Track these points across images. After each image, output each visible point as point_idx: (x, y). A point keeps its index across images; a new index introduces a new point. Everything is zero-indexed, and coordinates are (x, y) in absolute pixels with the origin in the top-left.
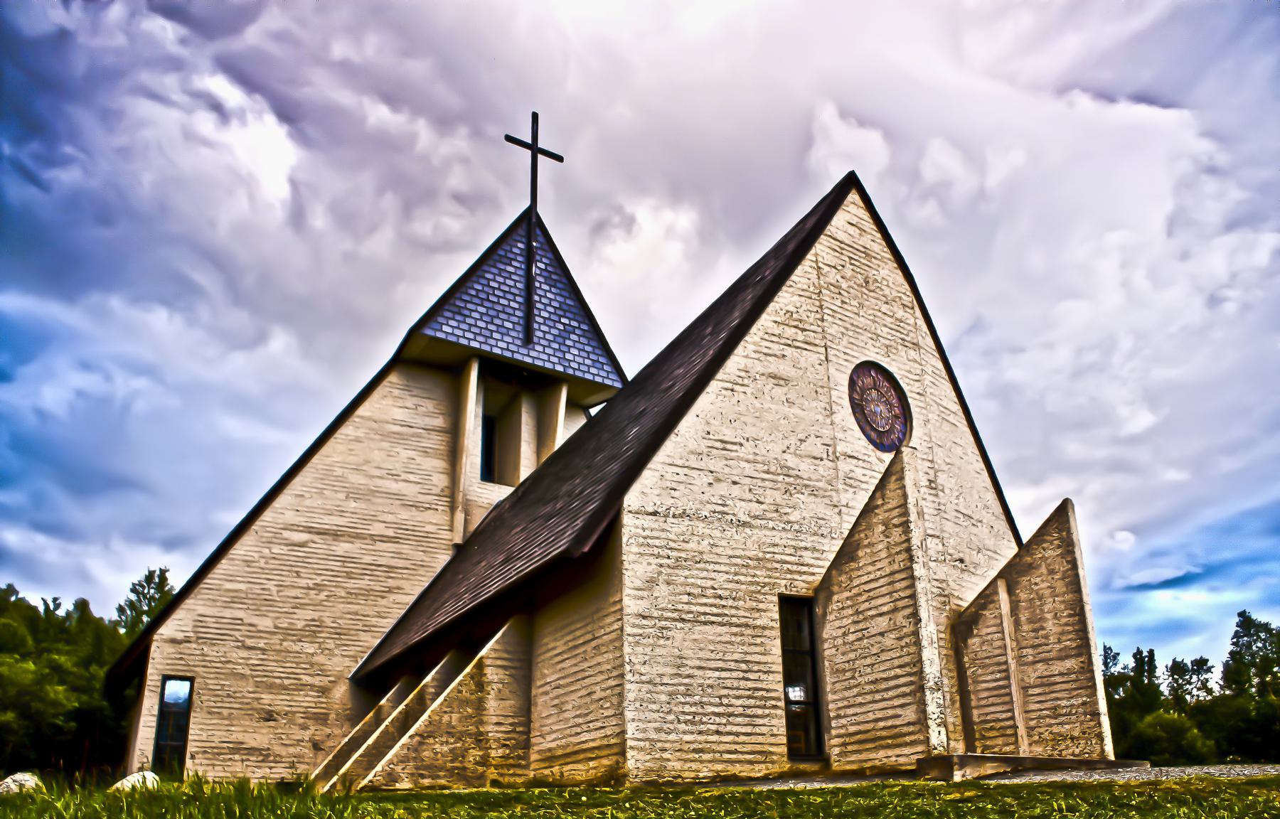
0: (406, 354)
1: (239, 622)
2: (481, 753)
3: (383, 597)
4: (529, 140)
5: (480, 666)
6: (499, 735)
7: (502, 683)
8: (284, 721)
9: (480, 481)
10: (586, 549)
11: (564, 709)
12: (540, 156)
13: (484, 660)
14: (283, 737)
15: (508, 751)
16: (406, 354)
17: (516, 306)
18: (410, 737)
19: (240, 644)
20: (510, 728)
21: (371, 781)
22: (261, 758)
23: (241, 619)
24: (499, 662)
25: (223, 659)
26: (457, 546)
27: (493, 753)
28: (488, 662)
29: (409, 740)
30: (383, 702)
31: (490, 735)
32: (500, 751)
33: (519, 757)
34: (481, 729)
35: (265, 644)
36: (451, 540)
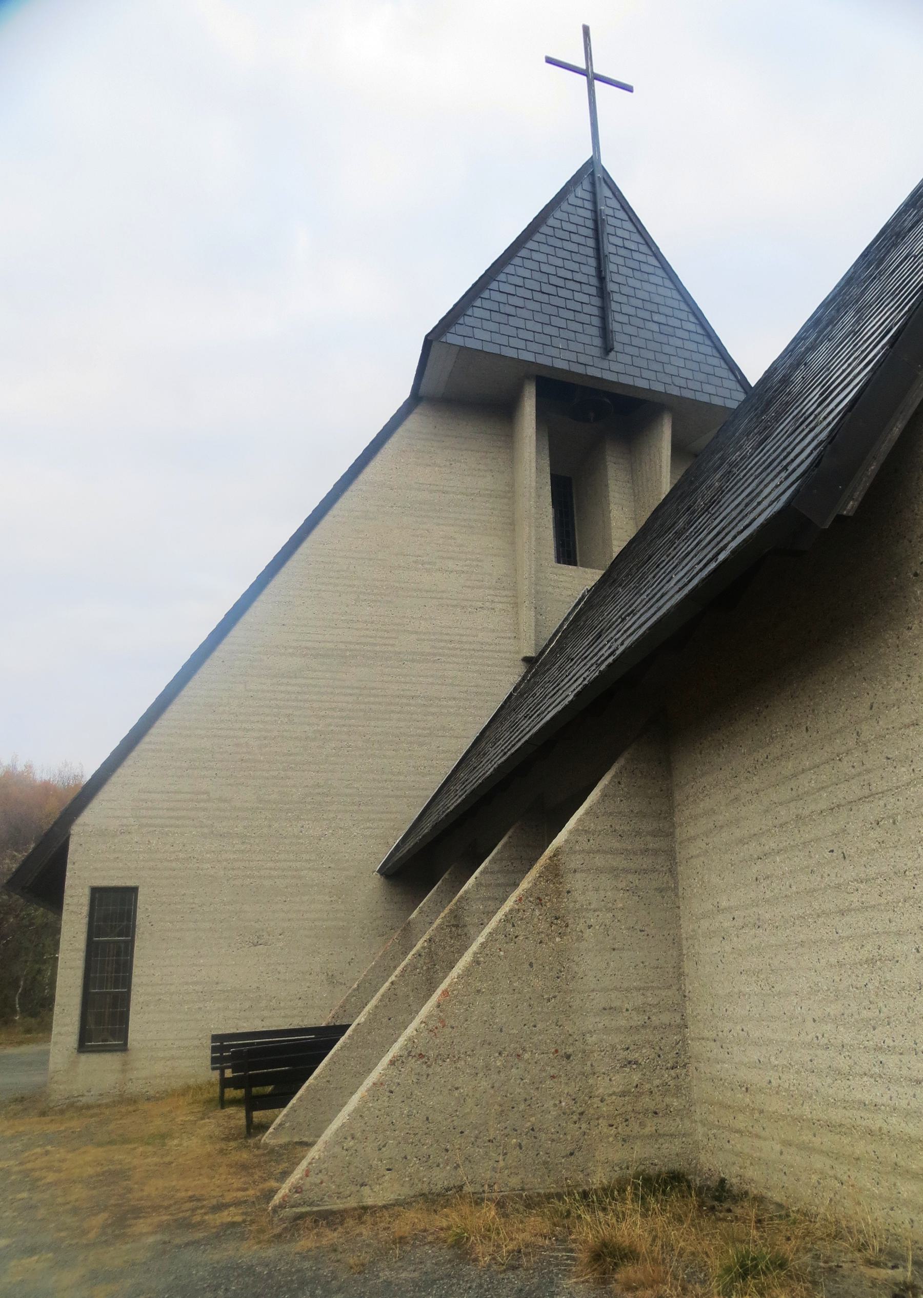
0: (423, 390)
1: (205, 797)
2: (572, 1089)
3: (421, 744)
4: (583, 66)
5: (554, 872)
6: (615, 1039)
7: (609, 910)
8: (281, 944)
9: (554, 563)
10: (850, 507)
11: (779, 988)
12: (596, 82)
13: (563, 858)
14: (280, 968)
15: (636, 1078)
16: (423, 390)
17: (585, 299)
18: (392, 1063)
19: (206, 830)
20: (637, 1019)
21: (297, 1189)
22: (247, 1005)
23: (207, 793)
24: (599, 861)
25: (181, 855)
26: (527, 660)
27: (602, 1087)
28: (574, 862)
29: (393, 1072)
30: (413, 916)
31: (591, 1040)
32: (617, 1078)
33: (665, 1089)
34: (568, 1028)
35: (245, 827)
36: (518, 653)
